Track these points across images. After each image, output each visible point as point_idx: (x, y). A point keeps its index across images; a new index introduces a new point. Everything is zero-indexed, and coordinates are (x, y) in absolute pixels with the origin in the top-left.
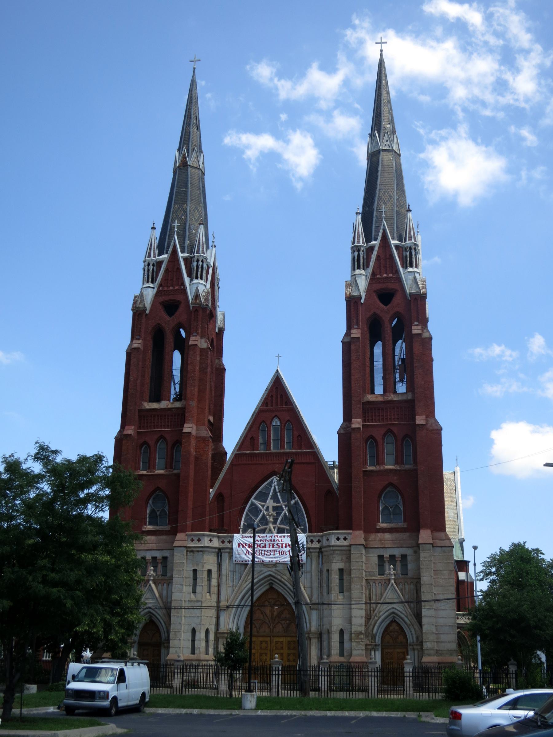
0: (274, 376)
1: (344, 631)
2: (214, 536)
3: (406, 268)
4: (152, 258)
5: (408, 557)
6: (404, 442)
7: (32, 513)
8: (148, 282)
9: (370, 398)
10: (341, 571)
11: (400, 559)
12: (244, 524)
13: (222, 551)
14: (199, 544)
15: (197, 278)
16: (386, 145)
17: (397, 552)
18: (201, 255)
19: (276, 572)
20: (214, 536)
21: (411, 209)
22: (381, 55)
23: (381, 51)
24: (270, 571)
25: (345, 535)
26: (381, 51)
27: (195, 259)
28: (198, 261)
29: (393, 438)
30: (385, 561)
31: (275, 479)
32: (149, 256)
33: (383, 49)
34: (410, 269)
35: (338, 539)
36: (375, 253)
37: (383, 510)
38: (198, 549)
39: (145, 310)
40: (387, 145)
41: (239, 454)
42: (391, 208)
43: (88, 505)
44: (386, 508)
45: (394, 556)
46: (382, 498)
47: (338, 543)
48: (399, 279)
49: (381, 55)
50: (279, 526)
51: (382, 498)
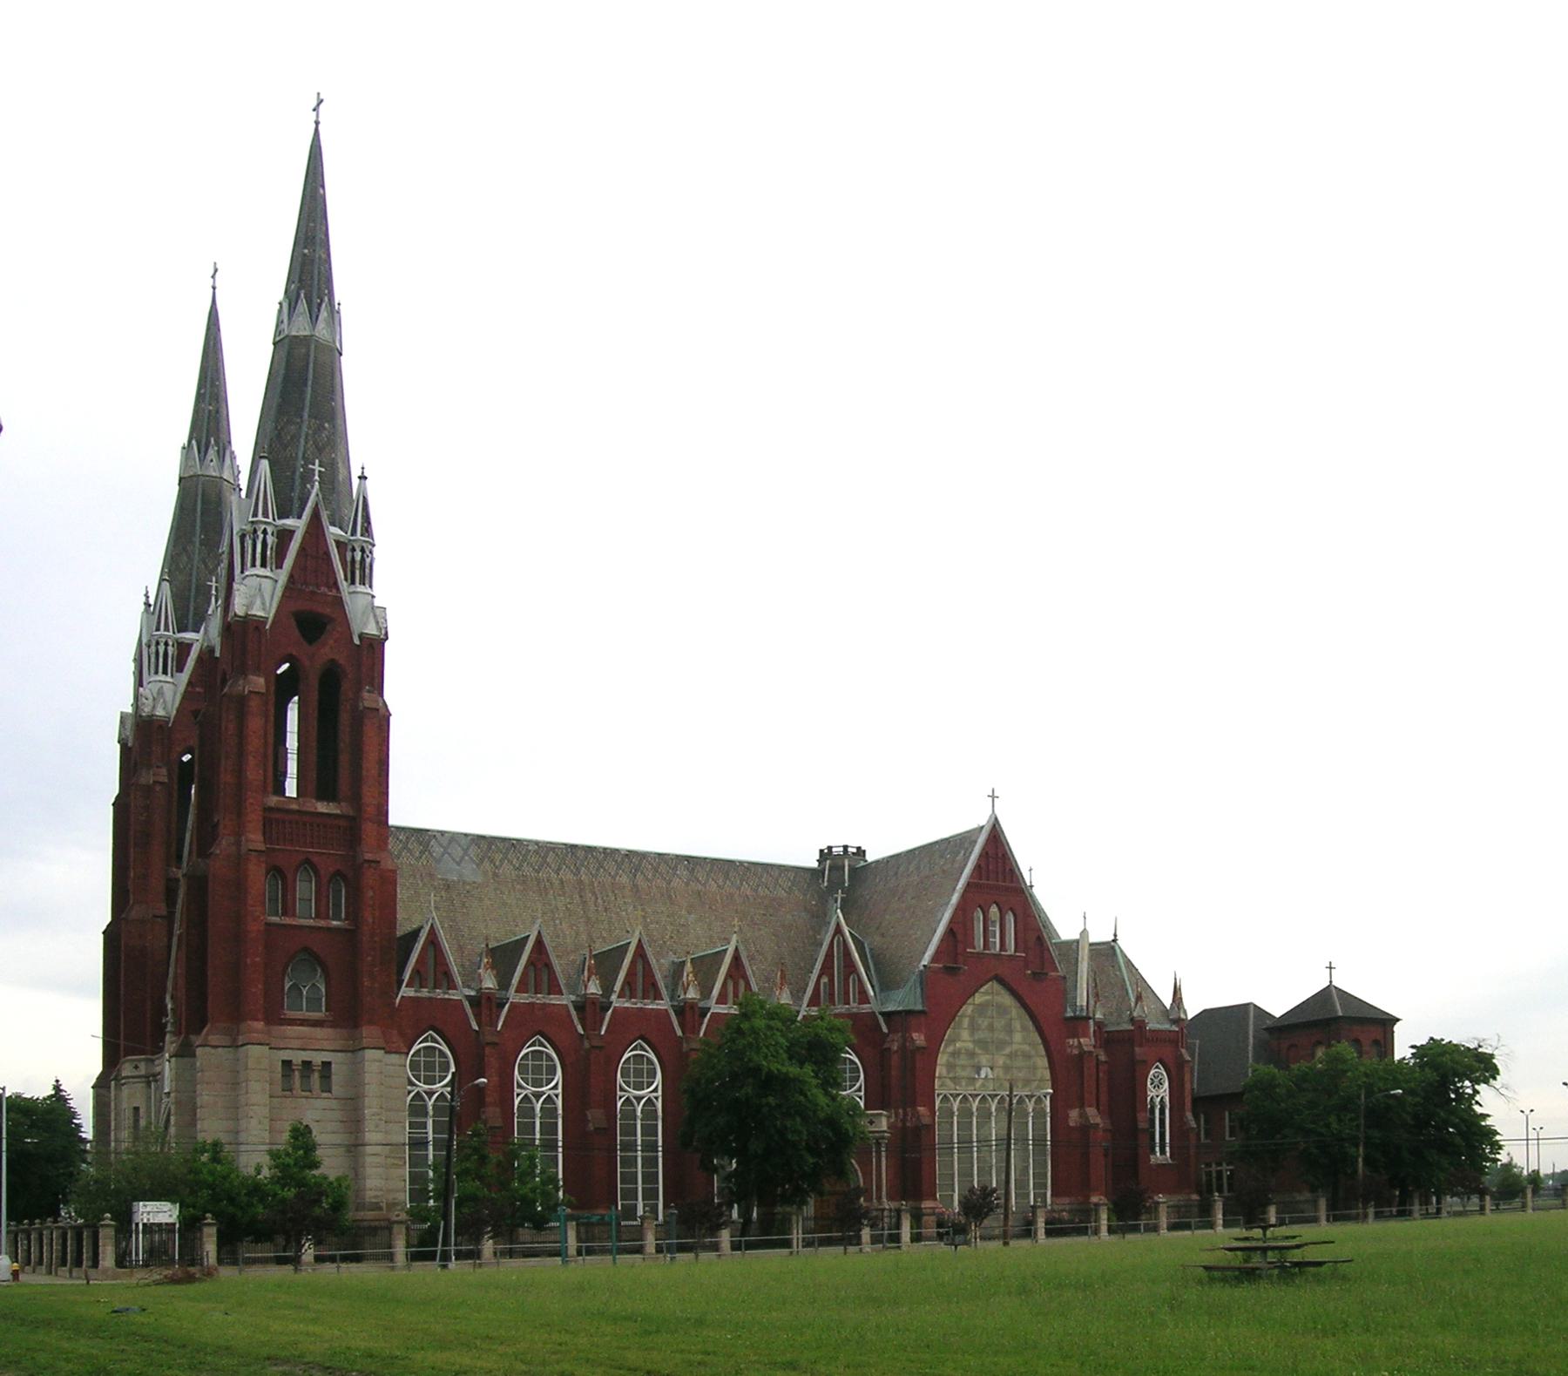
2: (140, 1060)
4: (162, 632)
5: (333, 1066)
6: (299, 874)
8: (156, 672)
9: (273, 800)
11: (320, 1068)
17: (318, 1058)
20: (140, 1060)
21: (365, 474)
22: (317, 130)
23: (317, 123)
26: (317, 123)
29: (312, 874)
30: (293, 1070)
32: (158, 629)
33: (320, 119)
34: (361, 588)
39: (167, 723)
43: (1147, 1028)
45: (310, 1063)
48: (339, 602)
49: (317, 130)
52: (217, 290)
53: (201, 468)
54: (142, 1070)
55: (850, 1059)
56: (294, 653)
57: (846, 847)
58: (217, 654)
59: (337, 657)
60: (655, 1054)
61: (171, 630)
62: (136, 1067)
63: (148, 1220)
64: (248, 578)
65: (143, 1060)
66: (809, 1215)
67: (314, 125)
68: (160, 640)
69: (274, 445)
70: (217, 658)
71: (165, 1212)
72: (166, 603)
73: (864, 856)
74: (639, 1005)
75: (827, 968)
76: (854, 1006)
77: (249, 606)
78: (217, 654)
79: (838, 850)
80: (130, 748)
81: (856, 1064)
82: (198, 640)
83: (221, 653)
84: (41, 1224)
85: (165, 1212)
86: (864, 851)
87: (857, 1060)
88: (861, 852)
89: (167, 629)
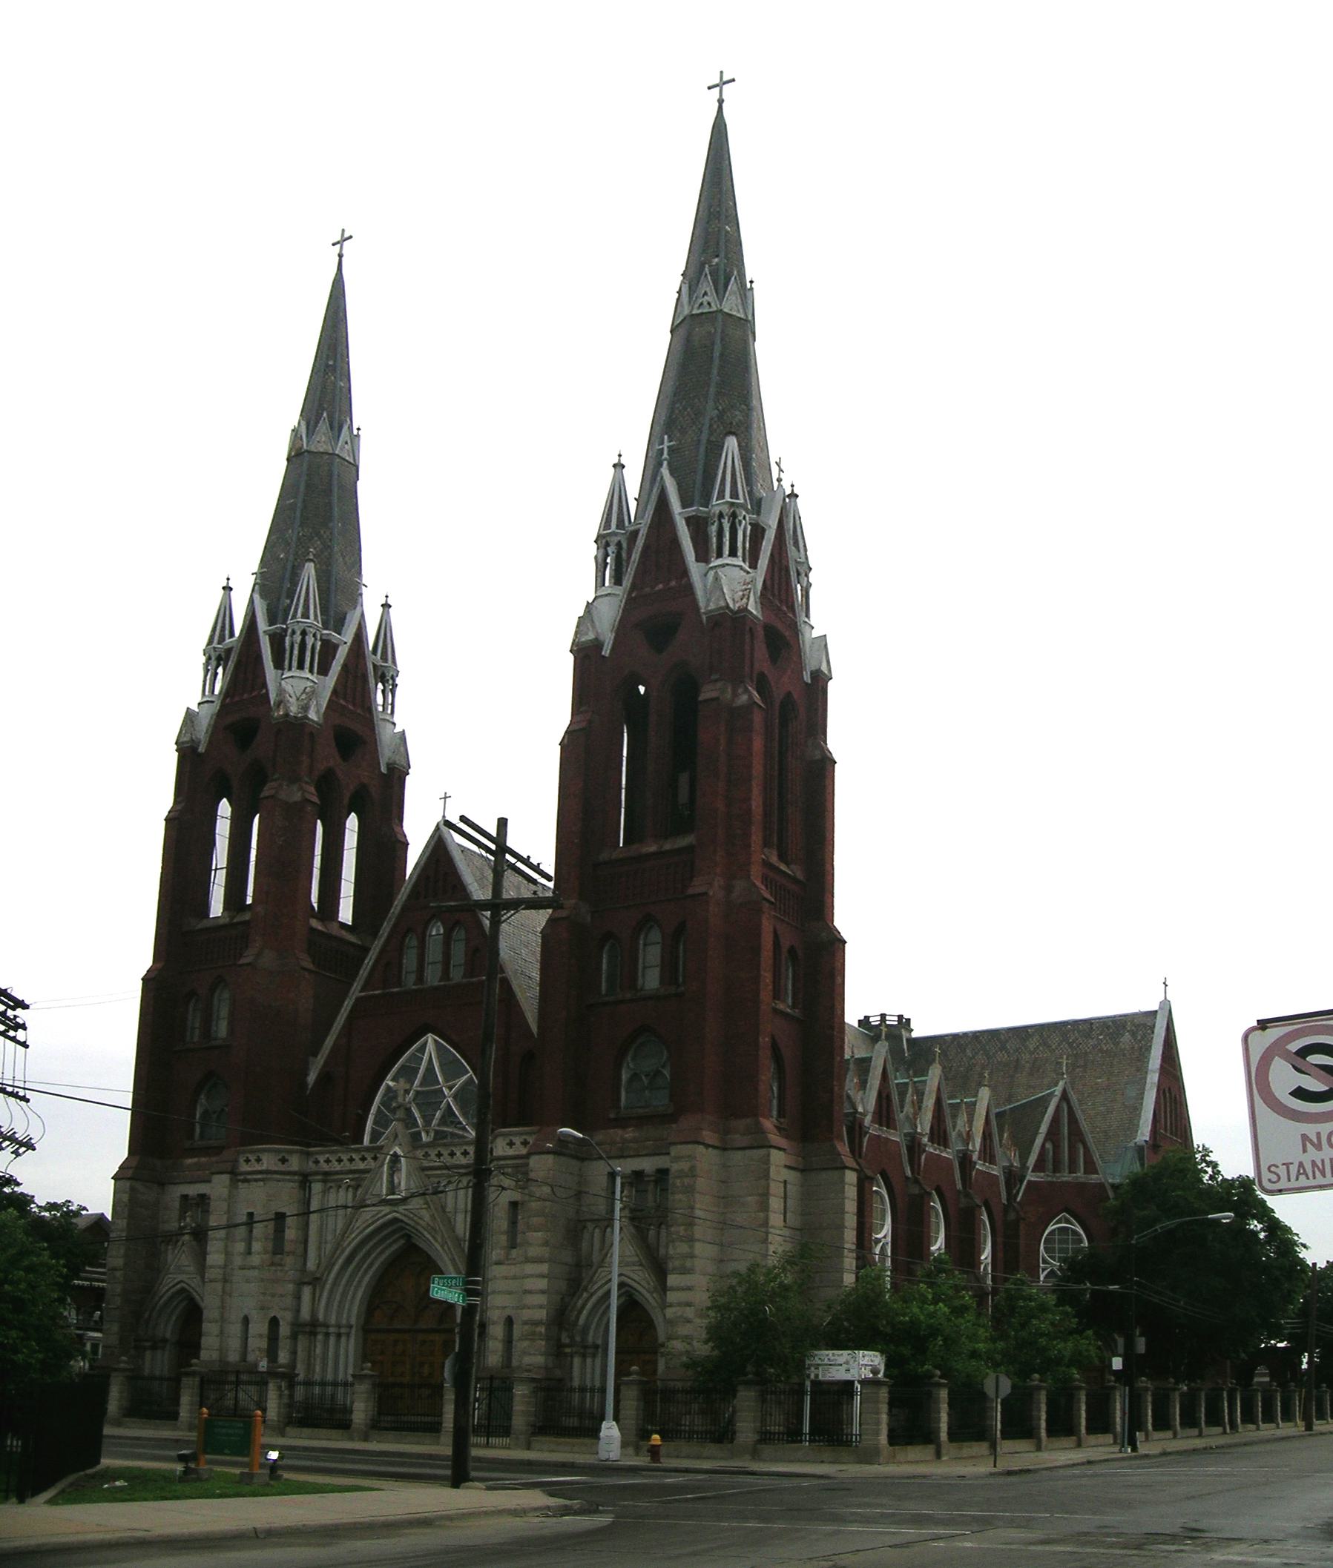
0: (432, 837)
1: (514, 1321)
2: (291, 1152)
3: (707, 561)
7: (1308, 1287)
10: (514, 1205)
12: (373, 1128)
13: (310, 1178)
14: (258, 1167)
15: (301, 667)
16: (702, 304)
18: (298, 622)
19: (406, 1213)
22: (720, 108)
24: (395, 1211)
25: (525, 1137)
27: (290, 631)
28: (304, 633)
31: (430, 1038)
35: (511, 1144)
36: (640, 542)
37: (630, 1081)
38: (255, 1177)
40: (705, 303)
41: (362, 997)
42: (695, 439)
44: (635, 1077)
46: (629, 1059)
47: (511, 1152)
49: (720, 108)
50: (437, 1128)
51: (629, 1059)
52: (343, 259)
53: (308, 442)
54: (295, 1163)
55: (1072, 1230)
56: (766, 672)
57: (883, 1016)
58: (606, 652)
59: (793, 692)
60: (942, 1205)
61: (312, 616)
62: (283, 1161)
63: (817, 1376)
64: (727, 567)
65: (297, 1151)
66: (341, 1376)
67: (717, 104)
68: (308, 629)
69: (715, 426)
70: (603, 657)
71: (841, 1365)
72: (308, 585)
73: (909, 1025)
74: (937, 1152)
75: (1053, 1134)
76: (1080, 1175)
77: (707, 605)
78: (606, 652)
79: (892, 1020)
80: (200, 755)
81: (1080, 1235)
82: (346, 643)
83: (610, 653)
84: (1041, 1381)
85: (841, 1365)
86: (908, 1020)
87: (1082, 1232)
88: (904, 1023)
89: (306, 615)
